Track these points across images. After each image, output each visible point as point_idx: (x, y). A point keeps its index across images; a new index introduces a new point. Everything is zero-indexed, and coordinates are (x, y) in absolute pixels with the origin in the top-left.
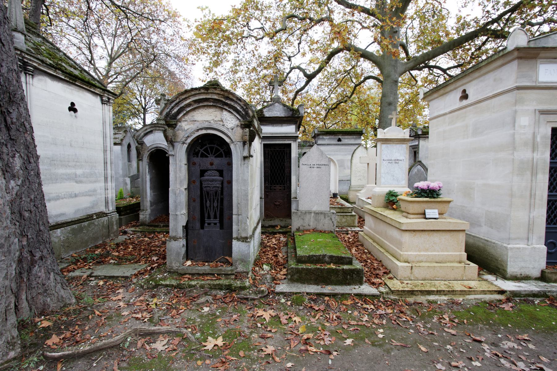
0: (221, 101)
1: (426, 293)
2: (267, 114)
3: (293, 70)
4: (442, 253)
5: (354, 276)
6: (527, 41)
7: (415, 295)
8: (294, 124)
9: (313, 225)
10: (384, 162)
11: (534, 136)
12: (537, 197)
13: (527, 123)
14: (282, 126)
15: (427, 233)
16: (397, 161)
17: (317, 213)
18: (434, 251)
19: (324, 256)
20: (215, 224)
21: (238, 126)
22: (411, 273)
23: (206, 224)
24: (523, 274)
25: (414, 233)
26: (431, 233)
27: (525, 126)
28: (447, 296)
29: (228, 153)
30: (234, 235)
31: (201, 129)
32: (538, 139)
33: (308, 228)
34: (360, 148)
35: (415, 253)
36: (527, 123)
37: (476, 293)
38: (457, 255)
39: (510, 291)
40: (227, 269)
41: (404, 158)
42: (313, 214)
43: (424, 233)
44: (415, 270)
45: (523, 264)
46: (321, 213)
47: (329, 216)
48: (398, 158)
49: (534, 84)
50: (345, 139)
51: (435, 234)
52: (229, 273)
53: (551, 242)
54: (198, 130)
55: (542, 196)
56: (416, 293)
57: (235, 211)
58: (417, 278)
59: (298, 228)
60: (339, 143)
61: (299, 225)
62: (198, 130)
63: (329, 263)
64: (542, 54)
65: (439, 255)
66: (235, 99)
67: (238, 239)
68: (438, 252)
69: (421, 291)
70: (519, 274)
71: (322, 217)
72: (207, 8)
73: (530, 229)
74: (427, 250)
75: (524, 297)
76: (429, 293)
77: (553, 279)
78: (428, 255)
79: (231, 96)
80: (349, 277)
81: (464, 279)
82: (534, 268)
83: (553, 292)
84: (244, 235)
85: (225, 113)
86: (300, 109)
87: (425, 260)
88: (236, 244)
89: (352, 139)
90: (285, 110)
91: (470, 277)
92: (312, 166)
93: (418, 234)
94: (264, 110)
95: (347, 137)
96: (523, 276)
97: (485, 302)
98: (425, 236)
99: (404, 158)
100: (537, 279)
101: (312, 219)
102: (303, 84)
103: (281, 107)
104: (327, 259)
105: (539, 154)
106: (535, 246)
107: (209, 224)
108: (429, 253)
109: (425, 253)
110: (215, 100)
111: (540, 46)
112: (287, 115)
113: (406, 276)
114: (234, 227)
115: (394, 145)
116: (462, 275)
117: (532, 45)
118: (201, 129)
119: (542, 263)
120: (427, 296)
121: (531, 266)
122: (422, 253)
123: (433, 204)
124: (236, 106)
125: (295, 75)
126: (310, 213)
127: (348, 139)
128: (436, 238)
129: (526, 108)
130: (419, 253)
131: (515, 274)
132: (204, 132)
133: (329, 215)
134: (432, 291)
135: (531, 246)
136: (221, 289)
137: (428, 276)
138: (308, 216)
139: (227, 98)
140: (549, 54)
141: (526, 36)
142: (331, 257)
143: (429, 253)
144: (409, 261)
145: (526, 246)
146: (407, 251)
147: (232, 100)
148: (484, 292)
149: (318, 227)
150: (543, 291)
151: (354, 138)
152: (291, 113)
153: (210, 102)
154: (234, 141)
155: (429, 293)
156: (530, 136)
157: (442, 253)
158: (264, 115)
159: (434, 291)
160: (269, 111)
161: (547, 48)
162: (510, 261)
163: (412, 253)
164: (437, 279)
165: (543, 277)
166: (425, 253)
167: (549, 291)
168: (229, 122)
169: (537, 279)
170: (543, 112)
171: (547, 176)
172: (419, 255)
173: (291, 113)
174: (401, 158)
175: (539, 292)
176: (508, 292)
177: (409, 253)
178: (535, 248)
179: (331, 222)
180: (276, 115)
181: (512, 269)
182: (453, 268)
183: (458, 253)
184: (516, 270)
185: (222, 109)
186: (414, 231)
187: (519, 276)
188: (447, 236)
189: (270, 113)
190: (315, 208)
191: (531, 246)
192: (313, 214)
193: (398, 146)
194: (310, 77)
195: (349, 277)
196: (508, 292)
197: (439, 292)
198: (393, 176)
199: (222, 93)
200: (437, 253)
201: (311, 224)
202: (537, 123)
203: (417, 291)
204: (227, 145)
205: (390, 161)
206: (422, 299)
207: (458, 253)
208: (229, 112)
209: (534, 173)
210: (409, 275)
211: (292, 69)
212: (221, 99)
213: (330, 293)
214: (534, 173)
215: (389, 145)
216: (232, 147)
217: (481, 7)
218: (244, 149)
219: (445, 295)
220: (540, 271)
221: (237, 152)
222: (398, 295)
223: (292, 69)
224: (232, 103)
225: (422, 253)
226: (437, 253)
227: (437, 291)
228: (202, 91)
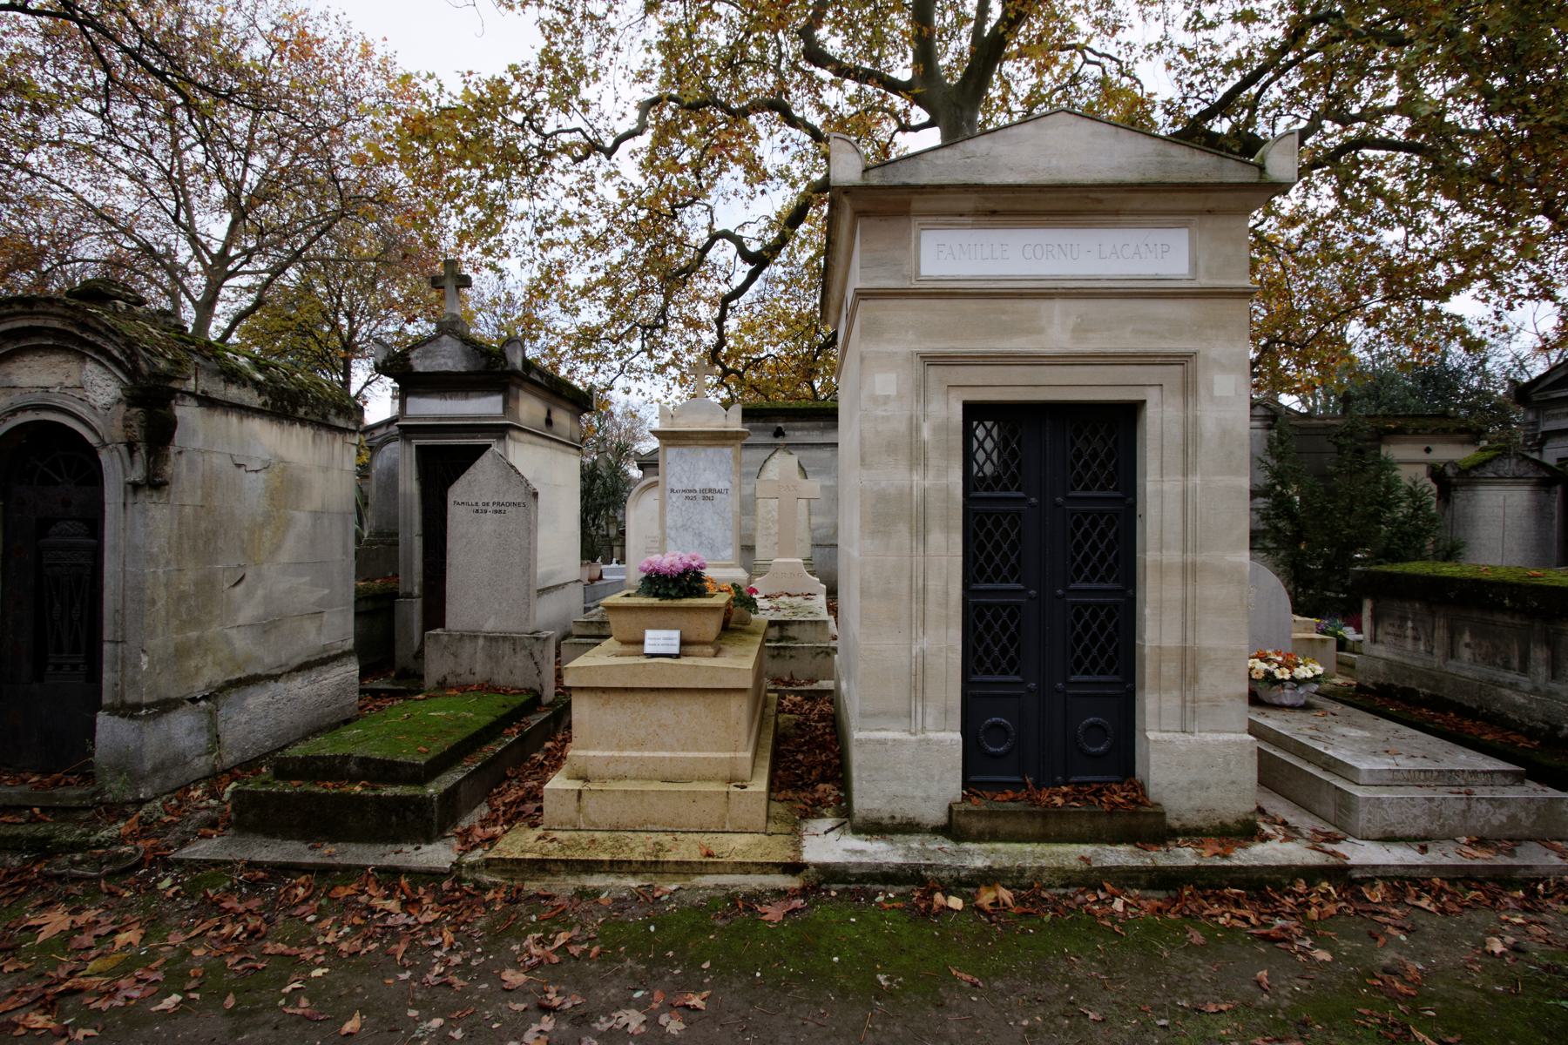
0: (72, 334)
1: (579, 868)
2: (420, 364)
3: (720, 242)
4: (682, 754)
5: (410, 816)
6: (860, 169)
7: (550, 873)
8: (499, 392)
9: (481, 671)
10: (674, 497)
11: (914, 428)
12: (931, 597)
13: (892, 391)
14: (467, 397)
15: (638, 697)
16: (708, 494)
17: (492, 639)
18: (663, 747)
19: (346, 758)
20: (75, 667)
21: (120, 400)
22: (579, 811)
23: (50, 668)
24: (898, 816)
25: (605, 696)
26: (653, 695)
27: (888, 397)
28: (641, 877)
29: (94, 477)
30: (107, 699)
31: (24, 409)
32: (926, 433)
33: (470, 678)
34: (777, 455)
35: (607, 754)
36: (892, 391)
37: (721, 869)
38: (722, 760)
39: (816, 865)
40: (73, 793)
41: (728, 485)
42: (481, 642)
43: (630, 696)
44: (590, 803)
45: (895, 787)
46: (505, 638)
47: (525, 648)
48: (713, 486)
49: (906, 284)
50: (794, 429)
51: (663, 700)
52: (75, 803)
53: (1092, 725)
54: (14, 413)
55: (947, 593)
56: (554, 868)
57: (107, 634)
58: (594, 824)
59: (440, 678)
60: (779, 441)
61: (445, 671)
62: (14, 413)
63: (354, 780)
64: (917, 204)
65: (671, 759)
66: (101, 328)
67: (114, 710)
68: (673, 750)
69: (566, 862)
70: (886, 815)
71: (507, 648)
72: (430, 76)
73: (918, 680)
74: (641, 745)
75: (858, 881)
76: (591, 867)
77: (974, 831)
78: (642, 759)
79: (92, 323)
80: (394, 818)
81: (728, 828)
82: (927, 799)
83: (941, 868)
84: (131, 698)
85: (90, 366)
86: (508, 350)
87: (633, 773)
88: (106, 726)
89: (813, 429)
90: (466, 354)
91: (744, 824)
92: (481, 507)
93: (616, 700)
94: (413, 355)
95: (799, 424)
96: (897, 821)
97: (732, 898)
98: (635, 705)
99: (728, 485)
100: (937, 831)
101: (480, 655)
102: (738, 279)
103: (457, 345)
104: (353, 767)
105: (931, 475)
106: (931, 735)
107: (58, 667)
108: (646, 754)
109: (634, 754)
110: (57, 333)
111: (896, 181)
112: (472, 369)
113: (564, 818)
114: (105, 676)
115: (700, 449)
116: (722, 817)
117: (875, 179)
118: (24, 409)
119: (951, 786)
120: (583, 876)
121: (919, 793)
122: (626, 754)
123: (672, 615)
124: (110, 347)
125: (723, 253)
126: (474, 637)
127: (802, 429)
128: (665, 711)
129: (890, 348)
130: (616, 754)
131: (875, 815)
132: (30, 417)
133: (527, 642)
134: (596, 862)
135: (920, 736)
136: (17, 850)
137: (625, 820)
138: (468, 647)
139: (84, 327)
140: (934, 203)
141: (856, 155)
142: (365, 762)
143: (646, 754)
144: (589, 773)
145: (904, 736)
146: (586, 748)
147: (97, 332)
148: (743, 868)
149: (496, 677)
150: (910, 866)
151: (818, 428)
152: (484, 361)
153: (47, 337)
154: (107, 440)
155: (591, 867)
156: (903, 427)
157: (682, 754)
158: (411, 367)
159: (602, 862)
160: (424, 356)
161: (924, 187)
162: (861, 779)
163: (598, 753)
164: (650, 827)
165: (952, 829)
166: (634, 754)
167: (929, 867)
168: (100, 391)
169: (937, 831)
170: (932, 360)
171: (957, 539)
172: (617, 760)
173: (484, 361)
174: (721, 485)
175: (900, 867)
176: (812, 869)
177: (591, 753)
178: (928, 741)
179: (531, 663)
180: (444, 369)
181: (868, 798)
182: (693, 797)
183: (728, 755)
184: (876, 804)
185: (83, 357)
186: (604, 690)
187: (886, 821)
188: (697, 706)
189: (427, 362)
190: (490, 625)
191: (920, 736)
192: (481, 642)
193: (710, 451)
194: (759, 261)
195: (394, 818)
196: (812, 869)
197: (616, 867)
198: (700, 535)
199: (69, 313)
200: (667, 754)
201: (478, 668)
202: (922, 390)
203: (556, 861)
204: (92, 452)
205: (690, 495)
206: (565, 885)
207: (728, 755)
208: (102, 364)
209: (921, 531)
210: (574, 815)
211: (714, 237)
212: (70, 329)
213: (315, 864)
214: (921, 531)
215: (685, 450)
216: (104, 456)
217: (1174, 73)
218: (132, 463)
219: (634, 874)
220: (945, 809)
221: (116, 471)
222: (503, 871)
223: (714, 237)
224: (100, 341)
225: (626, 754)
226: (667, 754)
227: (611, 862)
228: (18, 308)
